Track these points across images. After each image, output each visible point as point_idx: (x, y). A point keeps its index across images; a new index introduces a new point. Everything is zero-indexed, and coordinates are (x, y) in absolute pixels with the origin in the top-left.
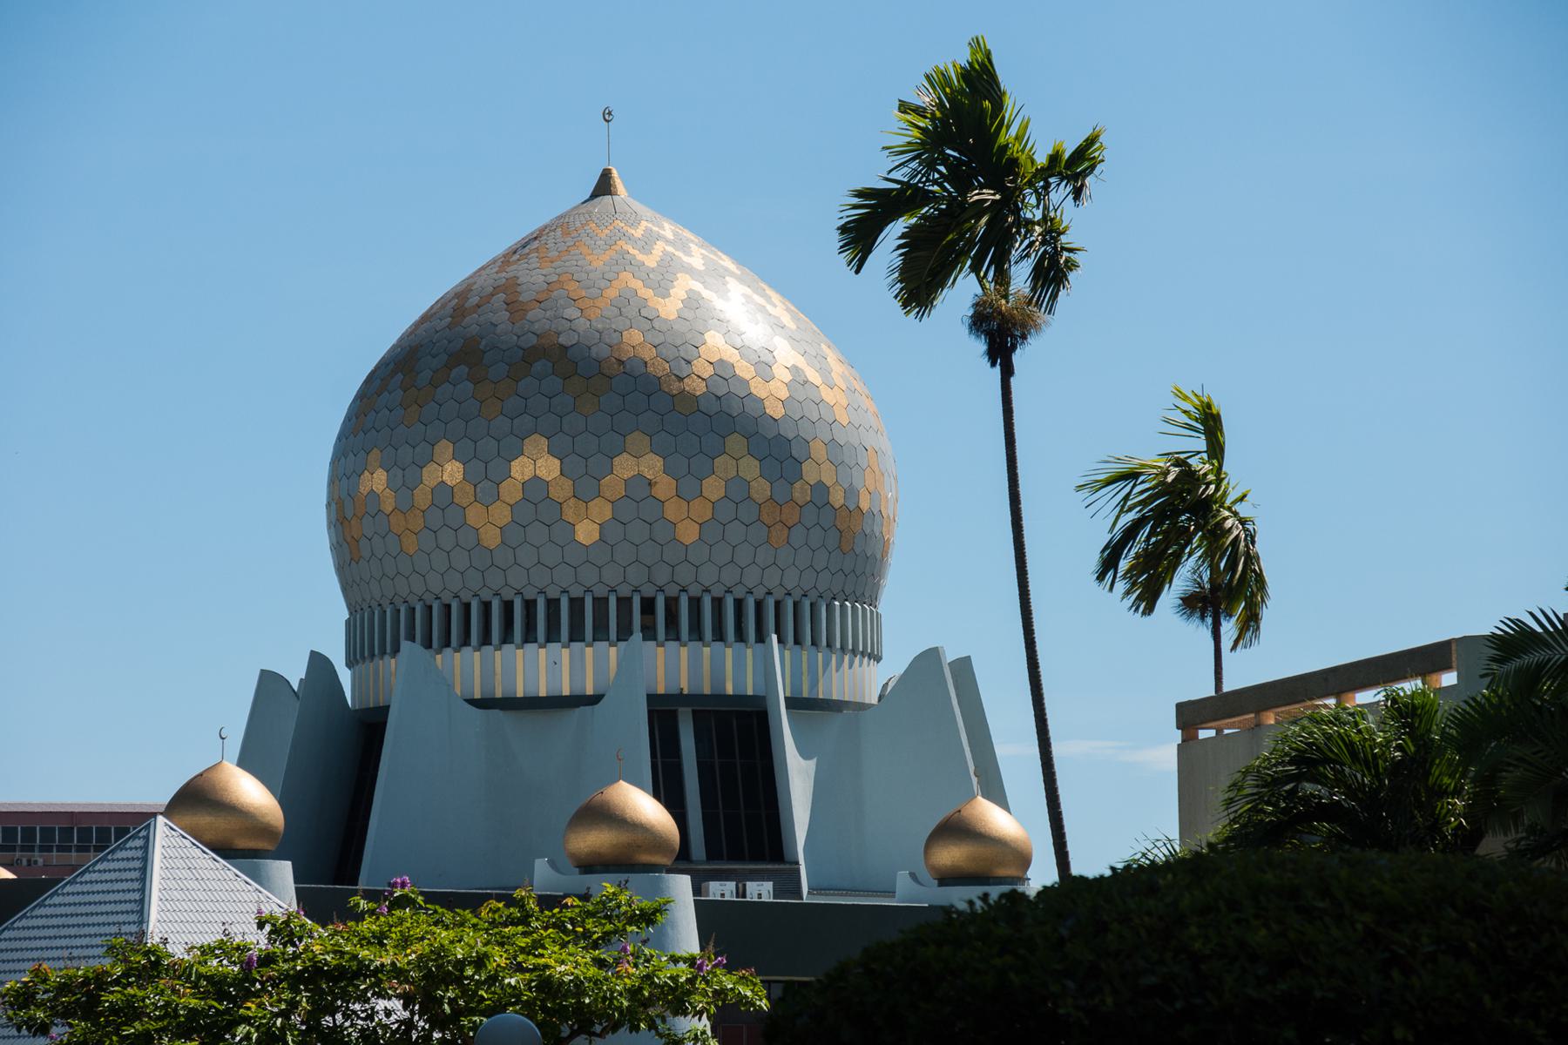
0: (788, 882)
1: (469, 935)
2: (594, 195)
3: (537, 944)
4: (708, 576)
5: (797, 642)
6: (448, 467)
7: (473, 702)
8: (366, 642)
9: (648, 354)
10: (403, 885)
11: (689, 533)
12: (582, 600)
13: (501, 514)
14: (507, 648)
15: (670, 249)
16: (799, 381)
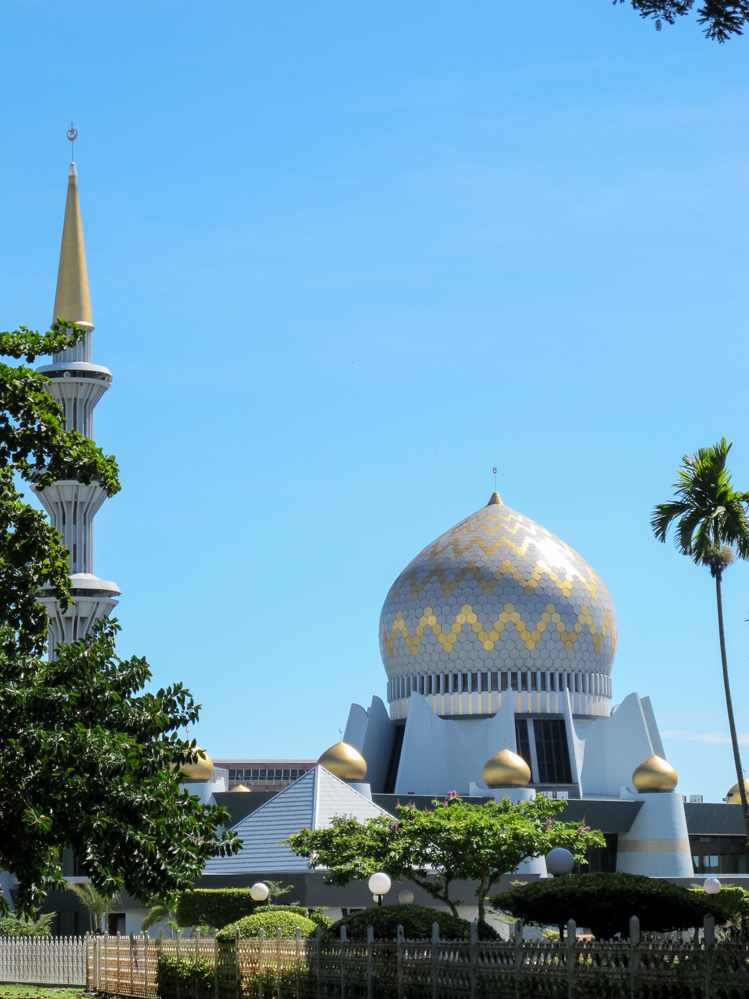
0: (574, 792)
1: (486, 817)
2: (489, 504)
3: (512, 819)
4: (539, 663)
5: (577, 691)
6: (430, 618)
7: (441, 717)
8: (398, 690)
9: (513, 570)
10: (454, 794)
11: (531, 645)
12: (497, 673)
13: (453, 638)
14: (455, 693)
15: (522, 526)
16: (576, 581)
